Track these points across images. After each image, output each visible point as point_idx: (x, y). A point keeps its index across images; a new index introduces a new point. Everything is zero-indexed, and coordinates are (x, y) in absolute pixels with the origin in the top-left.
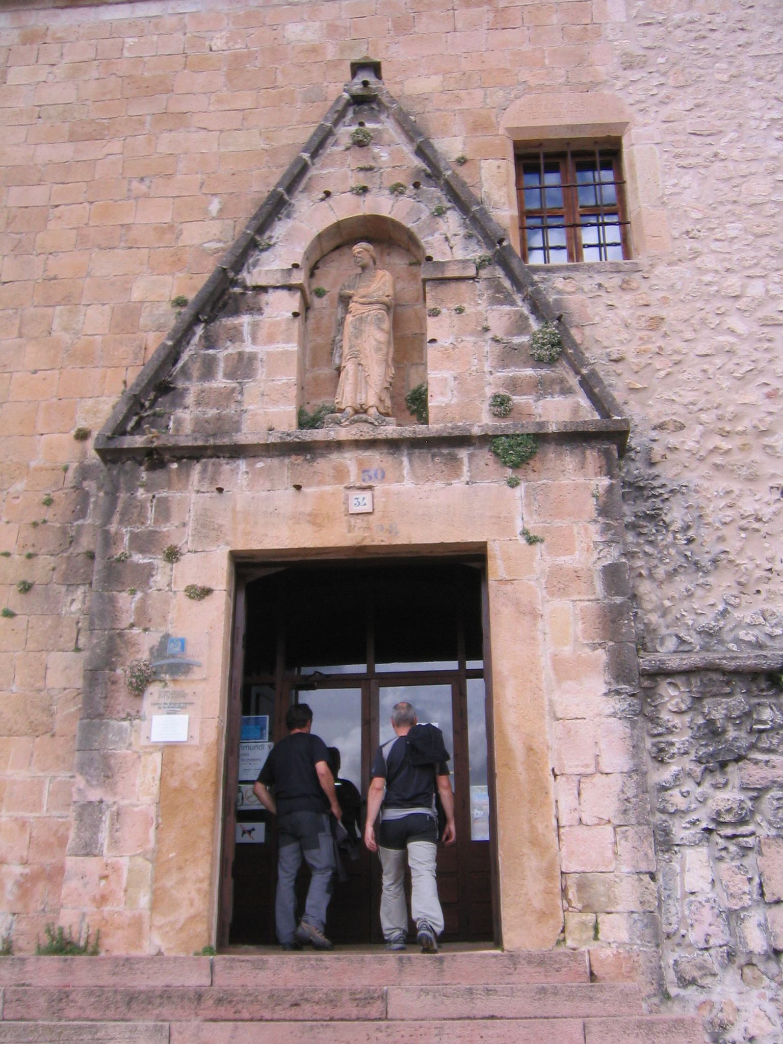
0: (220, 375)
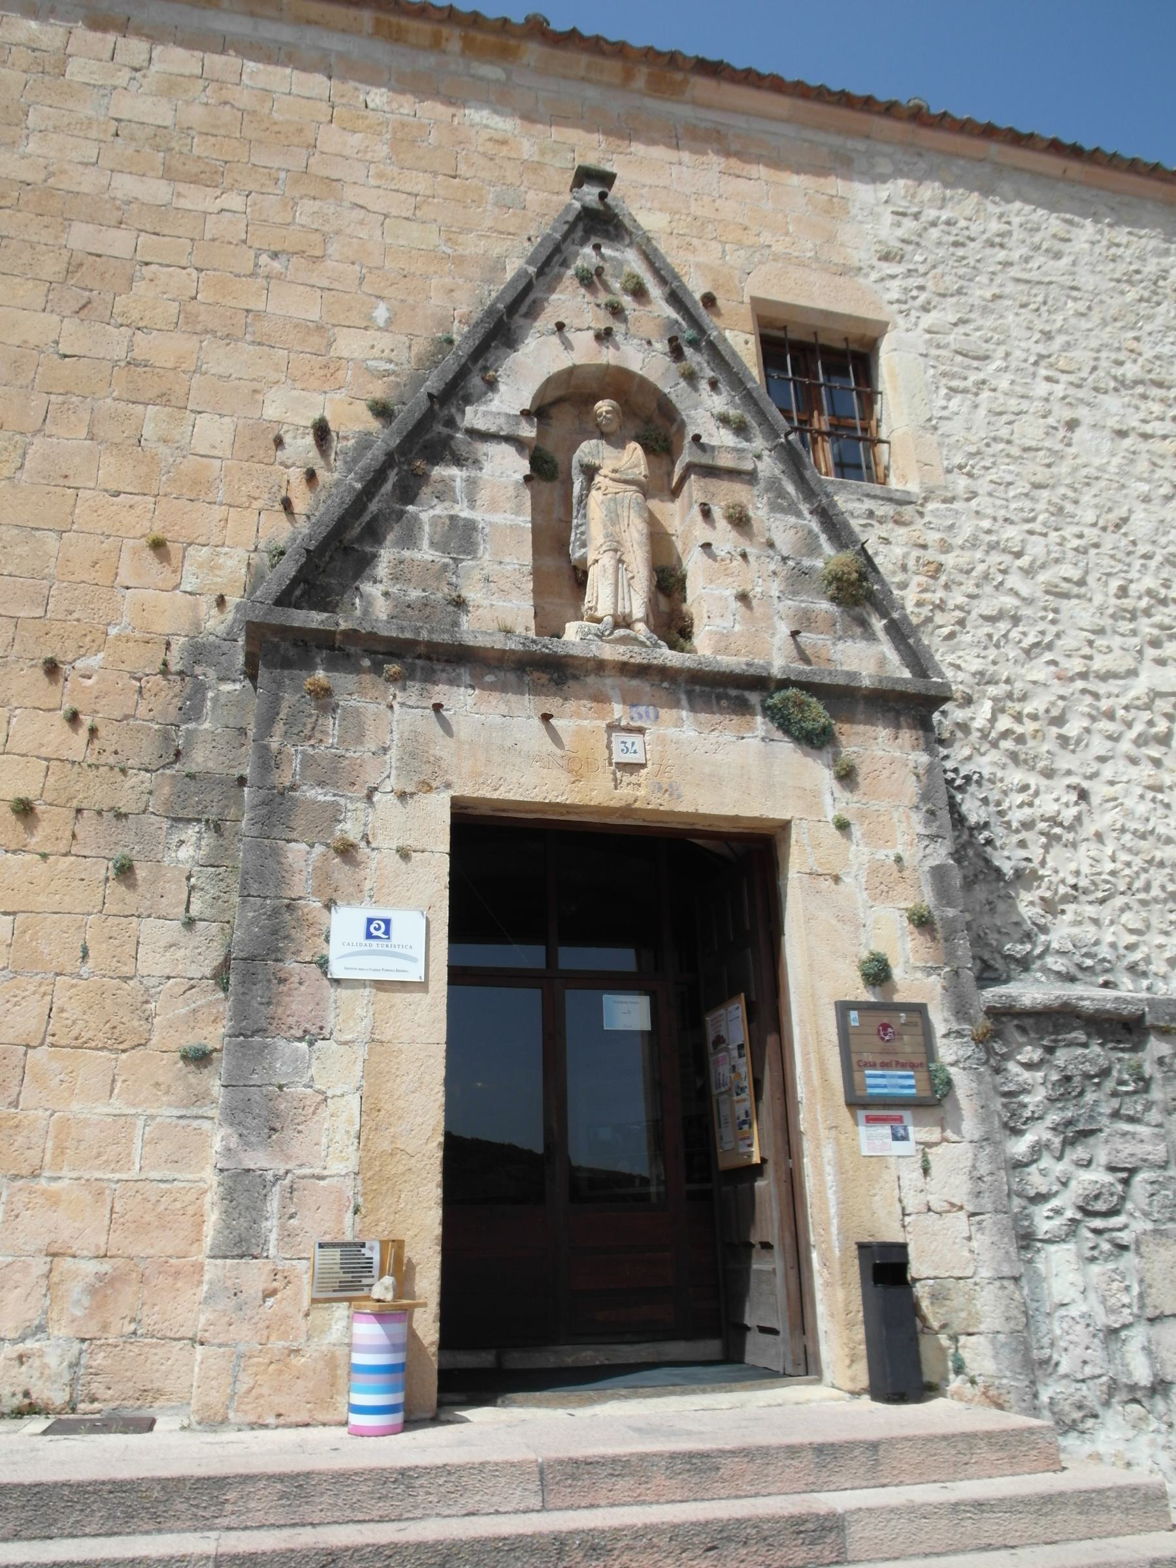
0: (425, 544)
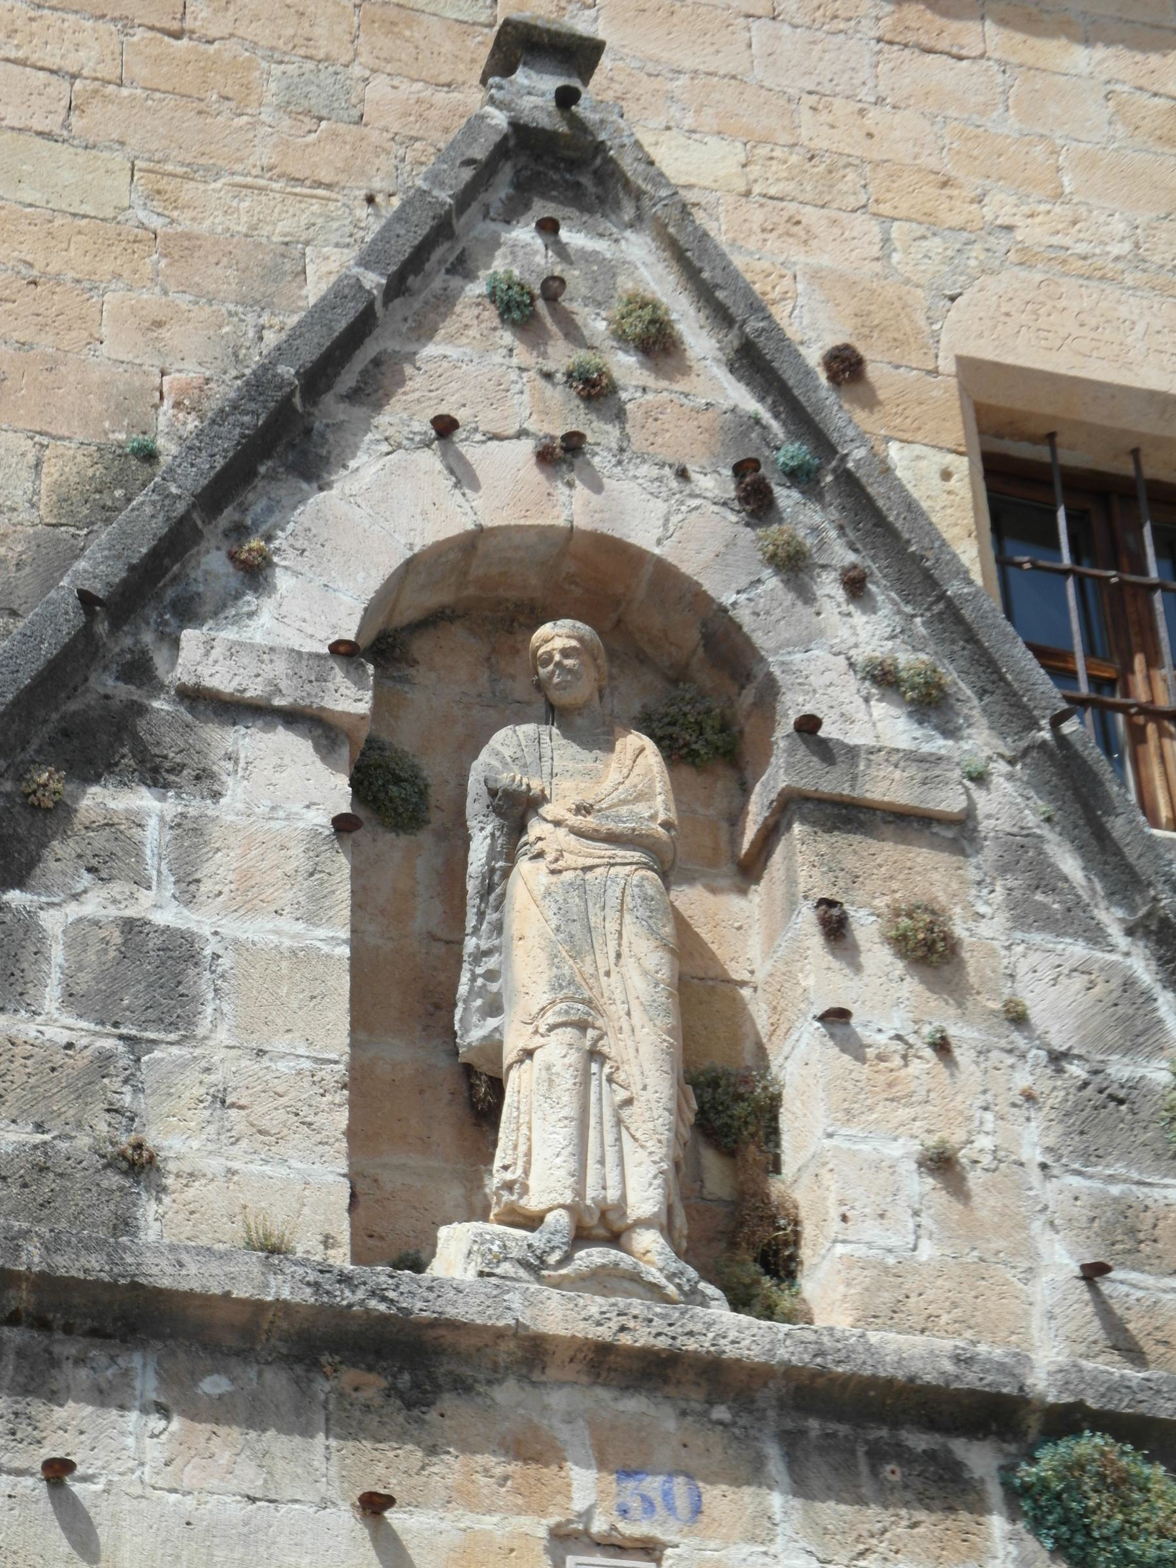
0: (51, 996)
